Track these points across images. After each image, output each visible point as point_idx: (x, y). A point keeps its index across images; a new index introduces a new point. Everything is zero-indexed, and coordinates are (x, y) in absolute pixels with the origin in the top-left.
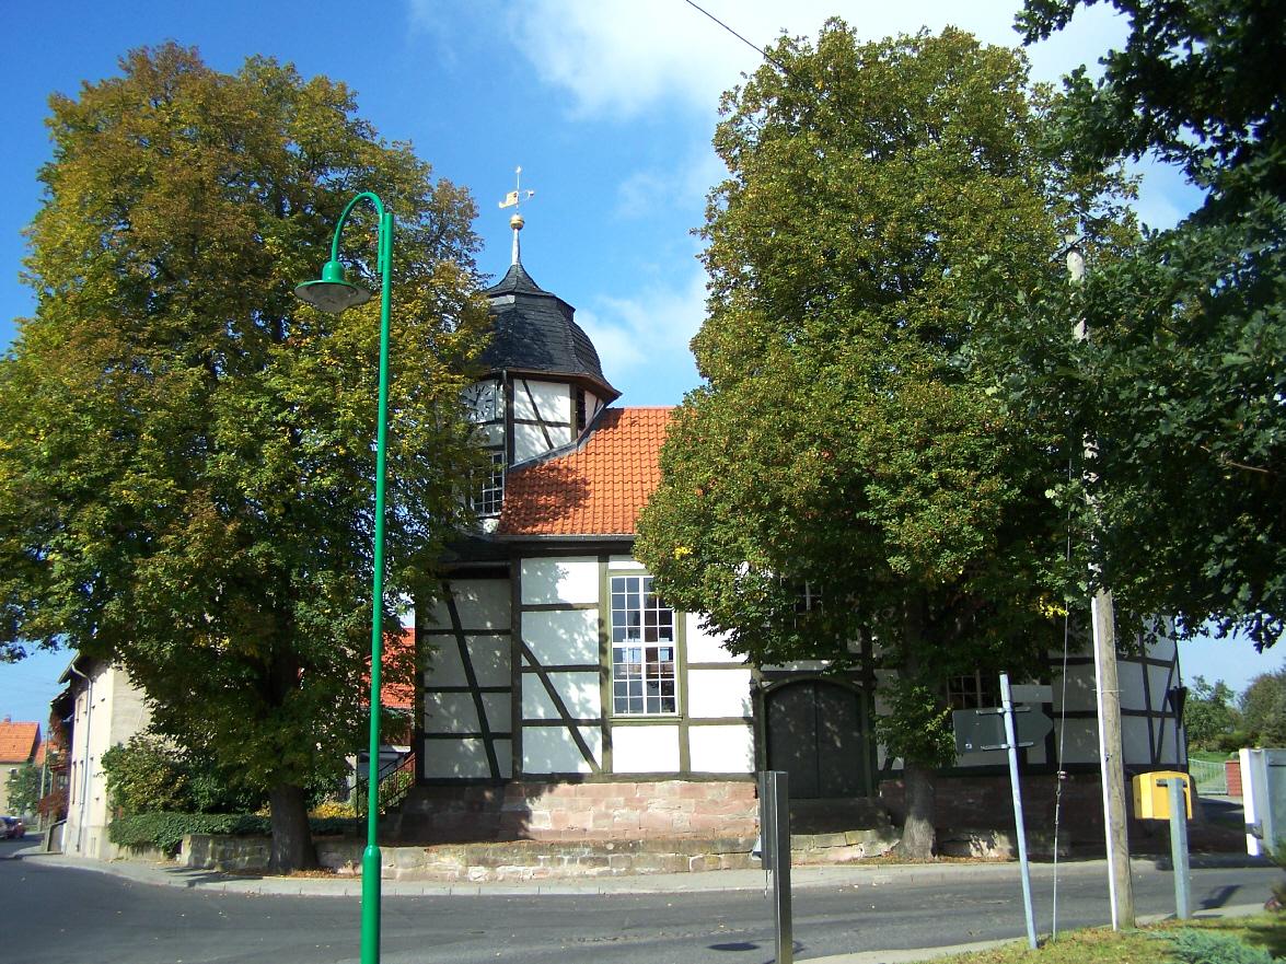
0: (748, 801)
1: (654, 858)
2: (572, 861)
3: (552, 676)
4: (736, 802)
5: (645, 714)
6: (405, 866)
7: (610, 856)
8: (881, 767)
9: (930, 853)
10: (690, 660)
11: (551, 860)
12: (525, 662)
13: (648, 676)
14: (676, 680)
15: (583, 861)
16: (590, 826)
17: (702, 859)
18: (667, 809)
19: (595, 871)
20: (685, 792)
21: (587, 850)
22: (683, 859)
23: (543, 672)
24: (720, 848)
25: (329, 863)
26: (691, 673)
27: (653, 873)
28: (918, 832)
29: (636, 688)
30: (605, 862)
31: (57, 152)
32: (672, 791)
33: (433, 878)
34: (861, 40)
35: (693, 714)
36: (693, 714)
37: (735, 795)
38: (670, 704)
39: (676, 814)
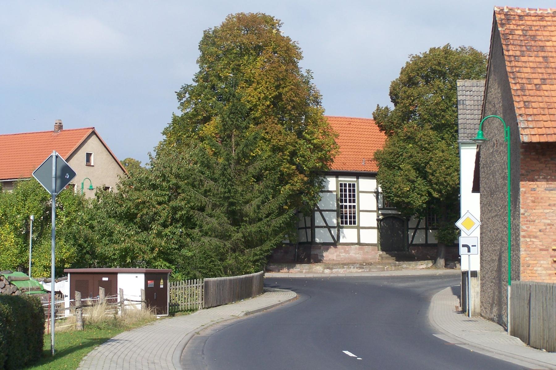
0: (376, 252)
1: (376, 267)
2: (354, 268)
3: (323, 213)
4: (373, 252)
5: (353, 225)
6: (306, 269)
7: (364, 267)
8: (410, 242)
9: (444, 267)
10: (361, 209)
11: (348, 268)
12: (316, 209)
13: (349, 214)
14: (356, 215)
15: (357, 268)
16: (335, 258)
17: (388, 267)
18: (355, 254)
19: (360, 270)
20: (360, 249)
21: (358, 265)
22: (384, 267)
23: (321, 211)
24: (392, 265)
25: (271, 269)
26: (361, 213)
27: (376, 271)
28: (441, 262)
29: (346, 218)
30: (363, 268)
31: (226, 19)
32: (356, 248)
33: (315, 273)
34: (145, 163)
35: (361, 225)
36: (361, 225)
37: (373, 250)
38: (354, 223)
39: (357, 255)
